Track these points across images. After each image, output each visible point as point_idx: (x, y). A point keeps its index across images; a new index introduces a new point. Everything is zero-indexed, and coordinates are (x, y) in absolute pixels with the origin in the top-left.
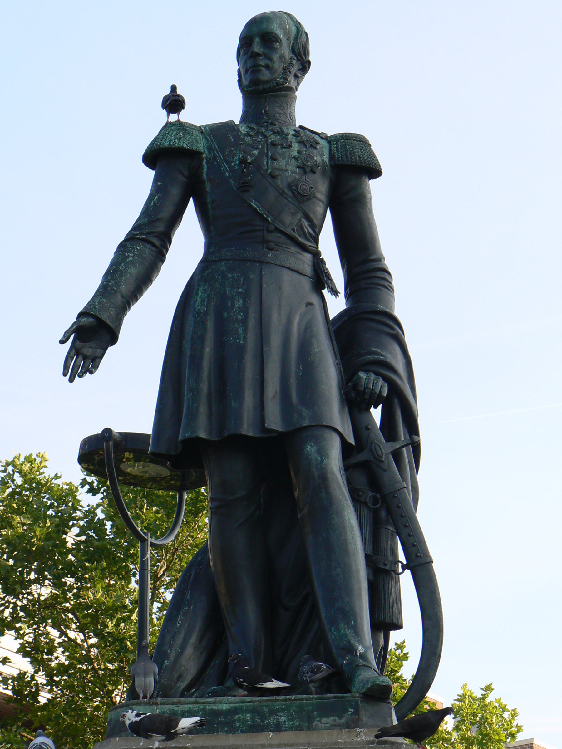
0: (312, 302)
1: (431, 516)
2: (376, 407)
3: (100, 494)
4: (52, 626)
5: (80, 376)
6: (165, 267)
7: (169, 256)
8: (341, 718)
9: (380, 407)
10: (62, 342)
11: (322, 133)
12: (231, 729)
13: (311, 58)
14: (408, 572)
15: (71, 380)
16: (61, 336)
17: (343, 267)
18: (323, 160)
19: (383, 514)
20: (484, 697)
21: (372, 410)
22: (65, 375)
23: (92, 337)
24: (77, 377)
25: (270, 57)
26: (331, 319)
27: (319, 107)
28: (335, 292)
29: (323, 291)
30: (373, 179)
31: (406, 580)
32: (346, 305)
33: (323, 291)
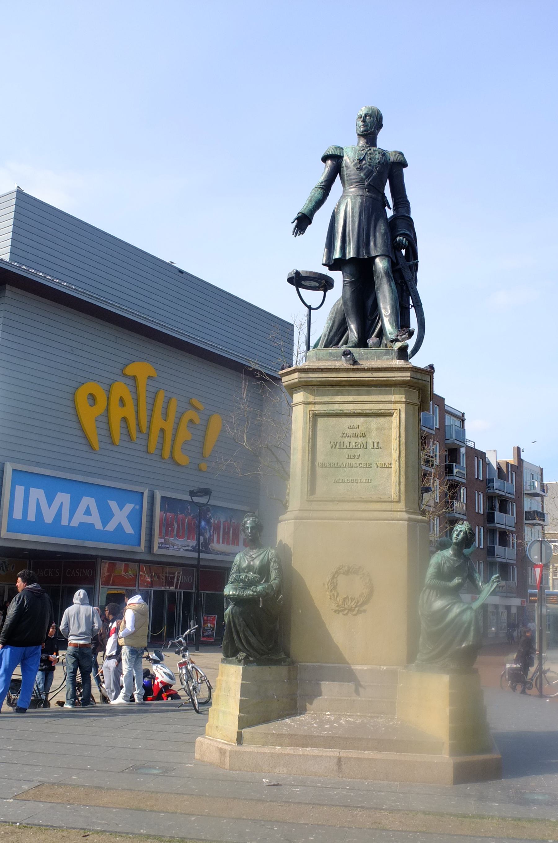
0: (493, 788)
1: (421, 287)
3: (229, 585)
4: (285, 329)
10: (293, 223)
13: (383, 123)
14: (413, 308)
19: (404, 288)
20: (526, 659)
21: (402, 250)
23: (303, 222)
25: (372, 126)
28: (390, 208)
31: (412, 311)
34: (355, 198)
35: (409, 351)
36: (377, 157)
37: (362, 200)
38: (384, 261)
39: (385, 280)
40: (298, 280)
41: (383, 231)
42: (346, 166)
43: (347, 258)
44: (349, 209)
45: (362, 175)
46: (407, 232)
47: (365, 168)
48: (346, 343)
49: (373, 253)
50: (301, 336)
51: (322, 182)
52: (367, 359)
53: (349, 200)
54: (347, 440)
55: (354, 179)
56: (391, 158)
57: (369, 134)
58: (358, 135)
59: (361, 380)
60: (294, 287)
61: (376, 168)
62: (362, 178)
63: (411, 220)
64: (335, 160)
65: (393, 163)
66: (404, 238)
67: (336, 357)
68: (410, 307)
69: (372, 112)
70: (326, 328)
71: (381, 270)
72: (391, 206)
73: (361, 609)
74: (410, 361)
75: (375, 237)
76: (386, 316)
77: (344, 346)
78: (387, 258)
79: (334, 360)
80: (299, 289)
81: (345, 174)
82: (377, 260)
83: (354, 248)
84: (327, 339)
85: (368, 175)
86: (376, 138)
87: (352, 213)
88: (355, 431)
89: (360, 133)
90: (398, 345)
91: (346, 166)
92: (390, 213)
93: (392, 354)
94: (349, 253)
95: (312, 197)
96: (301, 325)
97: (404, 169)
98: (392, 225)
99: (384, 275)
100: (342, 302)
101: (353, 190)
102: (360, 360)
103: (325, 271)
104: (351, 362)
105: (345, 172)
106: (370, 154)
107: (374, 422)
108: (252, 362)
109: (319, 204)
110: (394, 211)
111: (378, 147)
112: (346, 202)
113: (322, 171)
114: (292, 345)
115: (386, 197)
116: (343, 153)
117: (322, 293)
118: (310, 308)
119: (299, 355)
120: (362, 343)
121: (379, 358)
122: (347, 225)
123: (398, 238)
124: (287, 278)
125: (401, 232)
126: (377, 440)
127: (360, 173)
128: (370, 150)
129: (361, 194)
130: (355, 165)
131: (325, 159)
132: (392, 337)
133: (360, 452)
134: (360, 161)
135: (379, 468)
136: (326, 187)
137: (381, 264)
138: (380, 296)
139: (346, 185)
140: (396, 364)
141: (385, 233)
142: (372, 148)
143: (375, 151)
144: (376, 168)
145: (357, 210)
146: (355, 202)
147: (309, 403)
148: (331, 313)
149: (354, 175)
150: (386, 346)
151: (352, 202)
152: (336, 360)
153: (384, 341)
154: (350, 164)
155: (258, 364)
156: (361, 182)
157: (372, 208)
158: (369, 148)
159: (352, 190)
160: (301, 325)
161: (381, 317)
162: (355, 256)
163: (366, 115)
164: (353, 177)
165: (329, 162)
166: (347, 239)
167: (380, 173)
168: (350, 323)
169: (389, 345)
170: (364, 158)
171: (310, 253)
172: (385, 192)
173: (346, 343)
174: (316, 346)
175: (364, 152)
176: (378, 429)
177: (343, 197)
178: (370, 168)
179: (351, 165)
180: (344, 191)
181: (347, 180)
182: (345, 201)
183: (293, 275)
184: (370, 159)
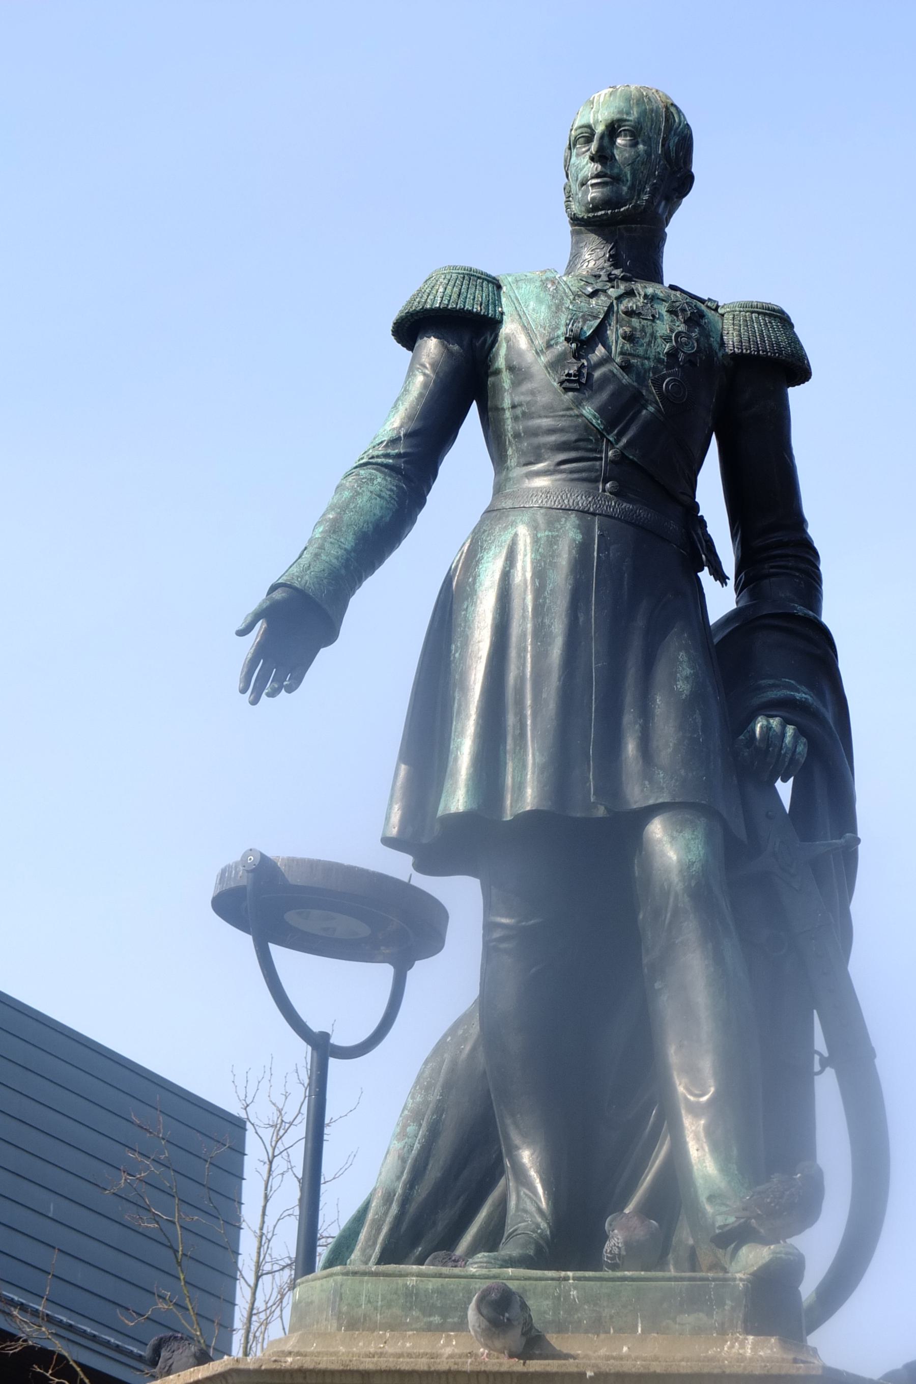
2: (785, 780)
4: (207, 1140)
5: (268, 695)
6: (424, 517)
7: (432, 497)
8: (709, 1314)
9: (792, 779)
10: (242, 633)
11: (710, 300)
13: (695, 169)
15: (255, 701)
16: (240, 624)
17: (734, 536)
18: (710, 345)
21: (779, 784)
22: (243, 691)
23: (295, 627)
24: (264, 695)
25: (639, 179)
26: (270, 945)
27: (711, 255)
29: (699, 574)
30: (793, 386)
31: (827, 1089)
32: (737, 603)
33: (699, 574)
34: (551, 524)
35: (808, 1288)
36: (663, 328)
37: (586, 531)
38: (687, 834)
39: (690, 931)
40: (274, 906)
41: (683, 687)
42: (511, 368)
43: (508, 817)
44: (523, 571)
45: (588, 411)
46: (803, 695)
47: (607, 379)
48: (491, 1239)
49: (637, 795)
50: (275, 1182)
51: (394, 441)
52: (598, 1326)
53: (523, 532)
55: (551, 431)
56: (732, 338)
57: (627, 218)
58: (575, 220)
60: (244, 942)
61: (658, 383)
62: (587, 426)
63: (825, 635)
64: (457, 333)
65: (740, 359)
66: (786, 721)
67: (442, 1314)
68: (817, 1067)
69: (643, 113)
70: (393, 1159)
71: (675, 878)
72: (729, 565)
74: (813, 1340)
75: (645, 712)
76: (695, 1110)
77: (481, 1256)
78: (702, 822)
79: (430, 1328)
80: (274, 948)
81: (507, 403)
82: (657, 829)
83: (542, 769)
84: (399, 1219)
85: (617, 414)
86: (662, 238)
87: (539, 593)
89: (581, 214)
90: (752, 1257)
91: (511, 368)
92: (720, 600)
93: (721, 1304)
94: (519, 787)
95: (343, 508)
96: (280, 1128)
97: (795, 394)
98: (731, 657)
99: (685, 901)
100: (475, 1030)
101: (542, 482)
102: (561, 1328)
103: (399, 866)
104: (515, 1338)
105: (508, 395)
106: (630, 313)
108: (23, 1307)
109: (375, 539)
110: (739, 589)
111: (667, 283)
112: (507, 537)
113: (396, 385)
114: (234, 1225)
115: (702, 523)
116: (497, 302)
117: (384, 972)
118: (323, 1048)
119: (266, 1280)
120: (572, 1240)
121: (654, 1324)
122: (513, 653)
123: (759, 726)
124: (210, 890)
125: (773, 694)
127: (578, 404)
128: (630, 293)
129: (582, 502)
130: (555, 365)
131: (409, 330)
132: (720, 1217)
134: (582, 344)
136: (414, 463)
137: (669, 847)
138: (667, 1006)
139: (512, 462)
140: (741, 1358)
141: (697, 699)
142: (638, 286)
143: (652, 299)
144: (658, 383)
145: (560, 578)
146: (552, 542)
148: (423, 1084)
149: (549, 410)
150: (693, 1262)
151: (536, 541)
152: (441, 1328)
153: (685, 1236)
154: (530, 357)
155: (50, 1319)
156: (580, 447)
157: (636, 558)
158: (622, 288)
159: (541, 483)
160: (280, 1128)
161: (669, 1119)
162: (545, 807)
163: (613, 129)
164: (545, 422)
165: (431, 346)
166: (511, 719)
167: (676, 408)
168: (516, 1139)
169: (705, 1256)
170: (599, 334)
171: (330, 773)
172: (701, 496)
173: (491, 1239)
174: (339, 1255)
175: (599, 304)
177: (494, 515)
178: (626, 379)
179: (538, 365)
180: (499, 489)
181: (517, 436)
182: (502, 531)
183: (242, 879)
184: (629, 338)
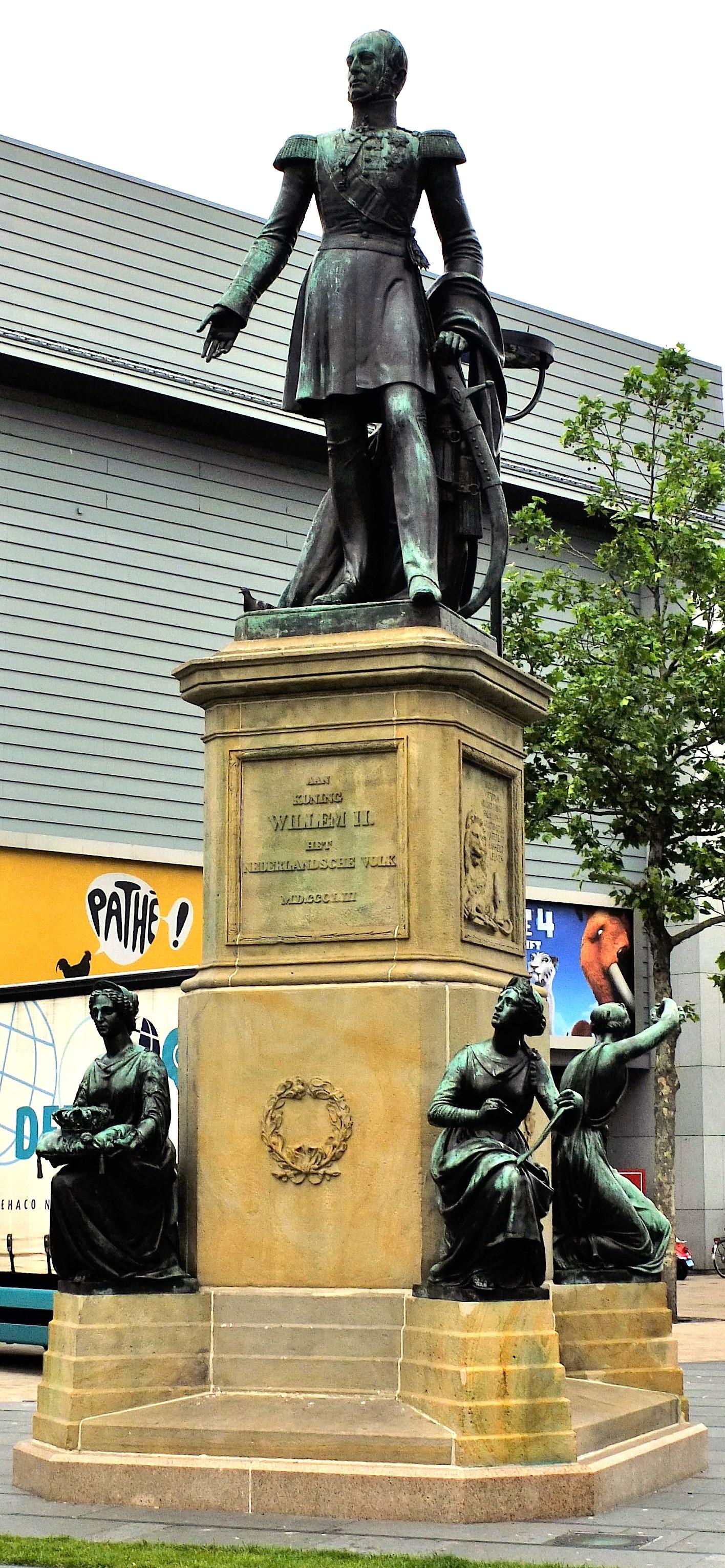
12: (317, 632)
19: (463, 445)
25: (377, 77)
54: (306, 810)
59: (323, 680)
73: (330, 1171)
88: (322, 790)
107: (360, 770)
126: (366, 809)
133: (332, 835)
135: (370, 868)
147: (226, 736)
176: (368, 783)
